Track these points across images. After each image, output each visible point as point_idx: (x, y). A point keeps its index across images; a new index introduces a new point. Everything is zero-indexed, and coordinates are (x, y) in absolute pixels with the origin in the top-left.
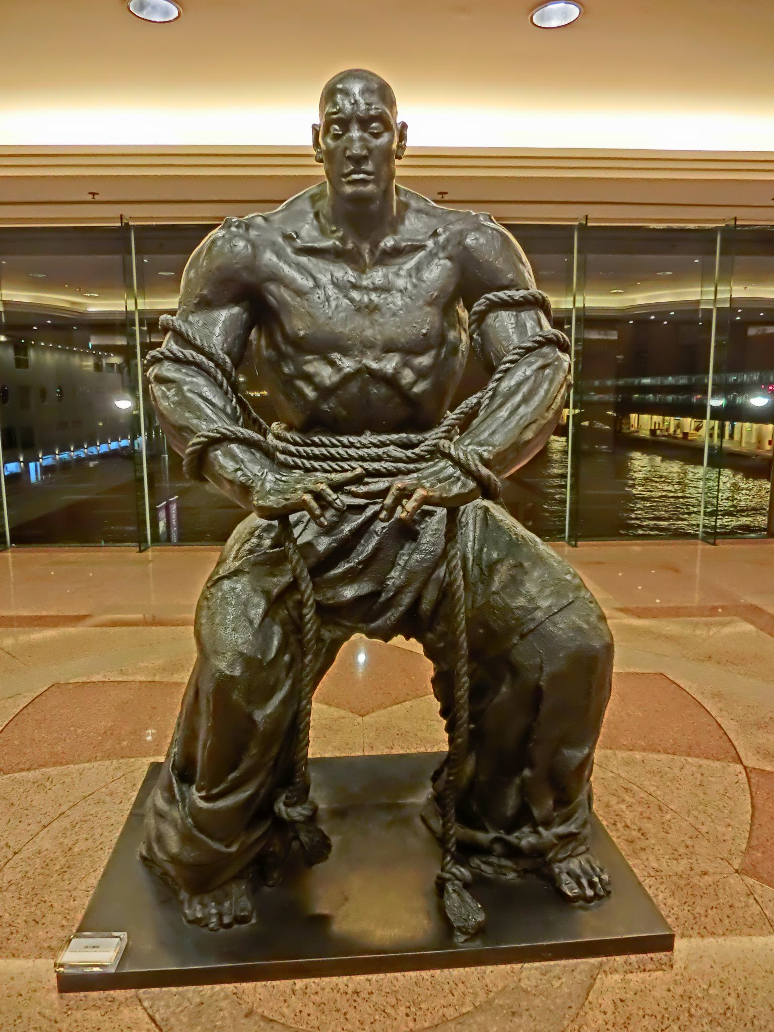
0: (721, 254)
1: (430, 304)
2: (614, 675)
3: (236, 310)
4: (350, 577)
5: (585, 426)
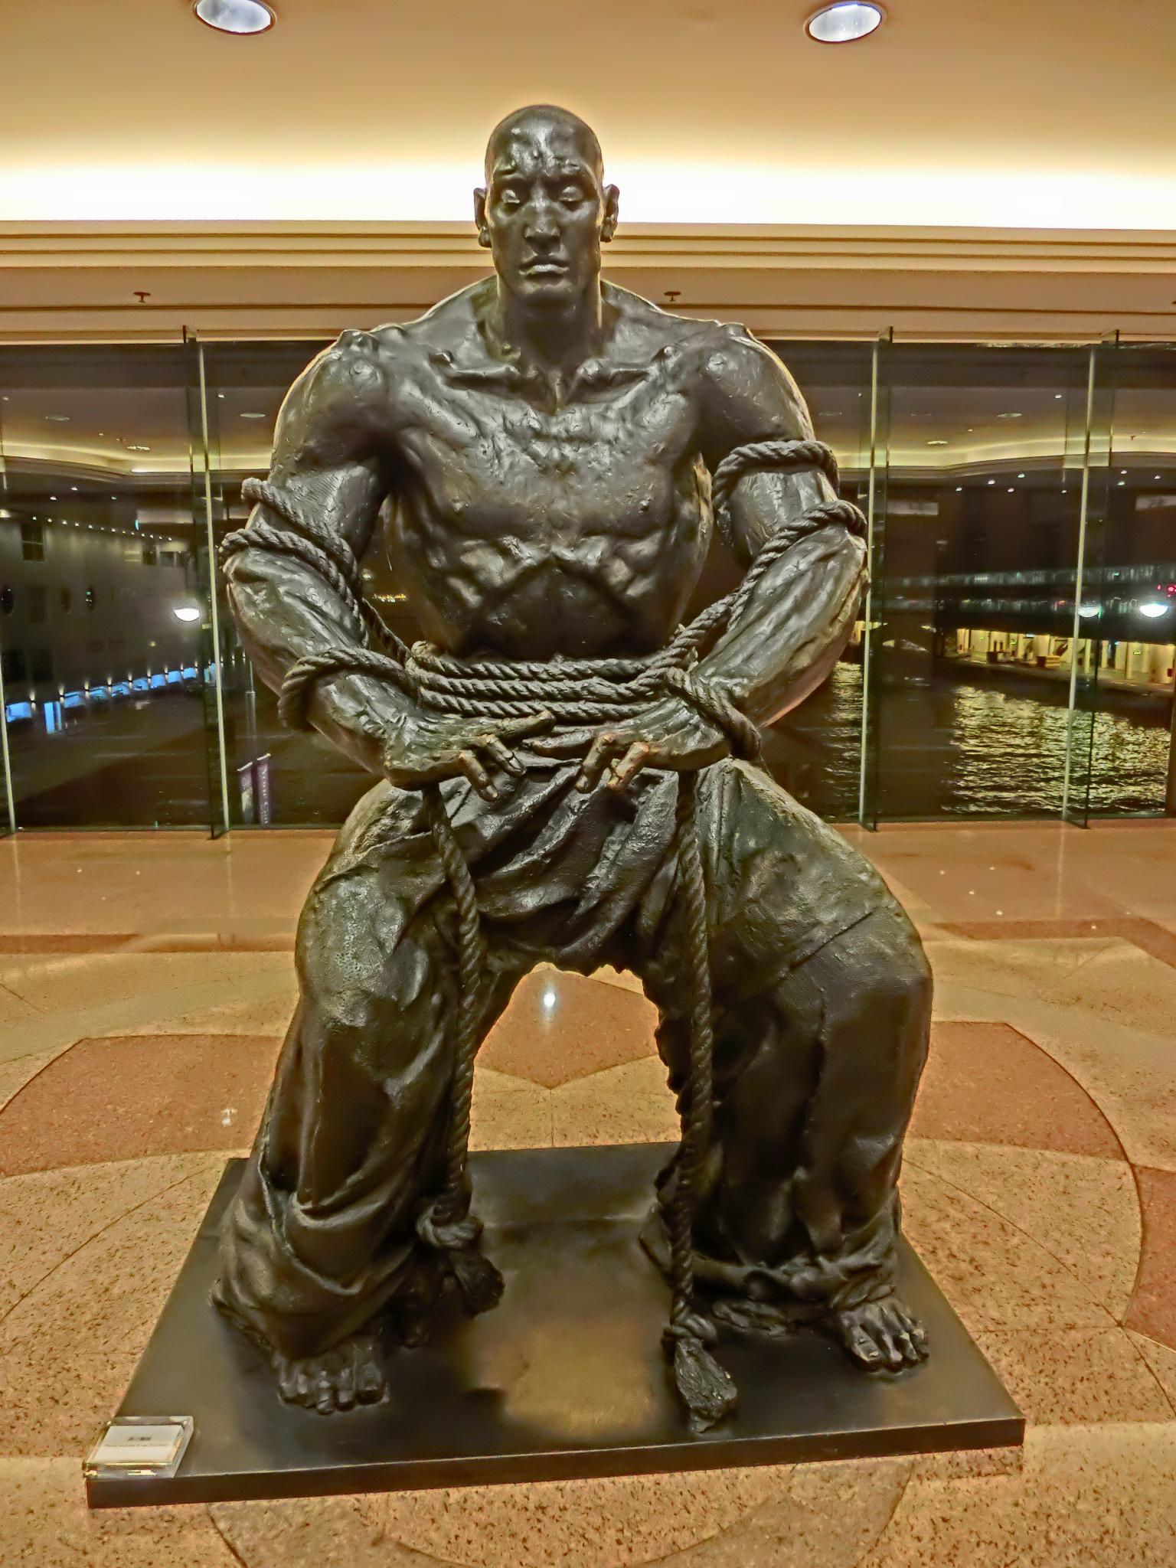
0: (1095, 386)
1: (653, 462)
3: (358, 471)
4: (532, 877)
5: (889, 647)
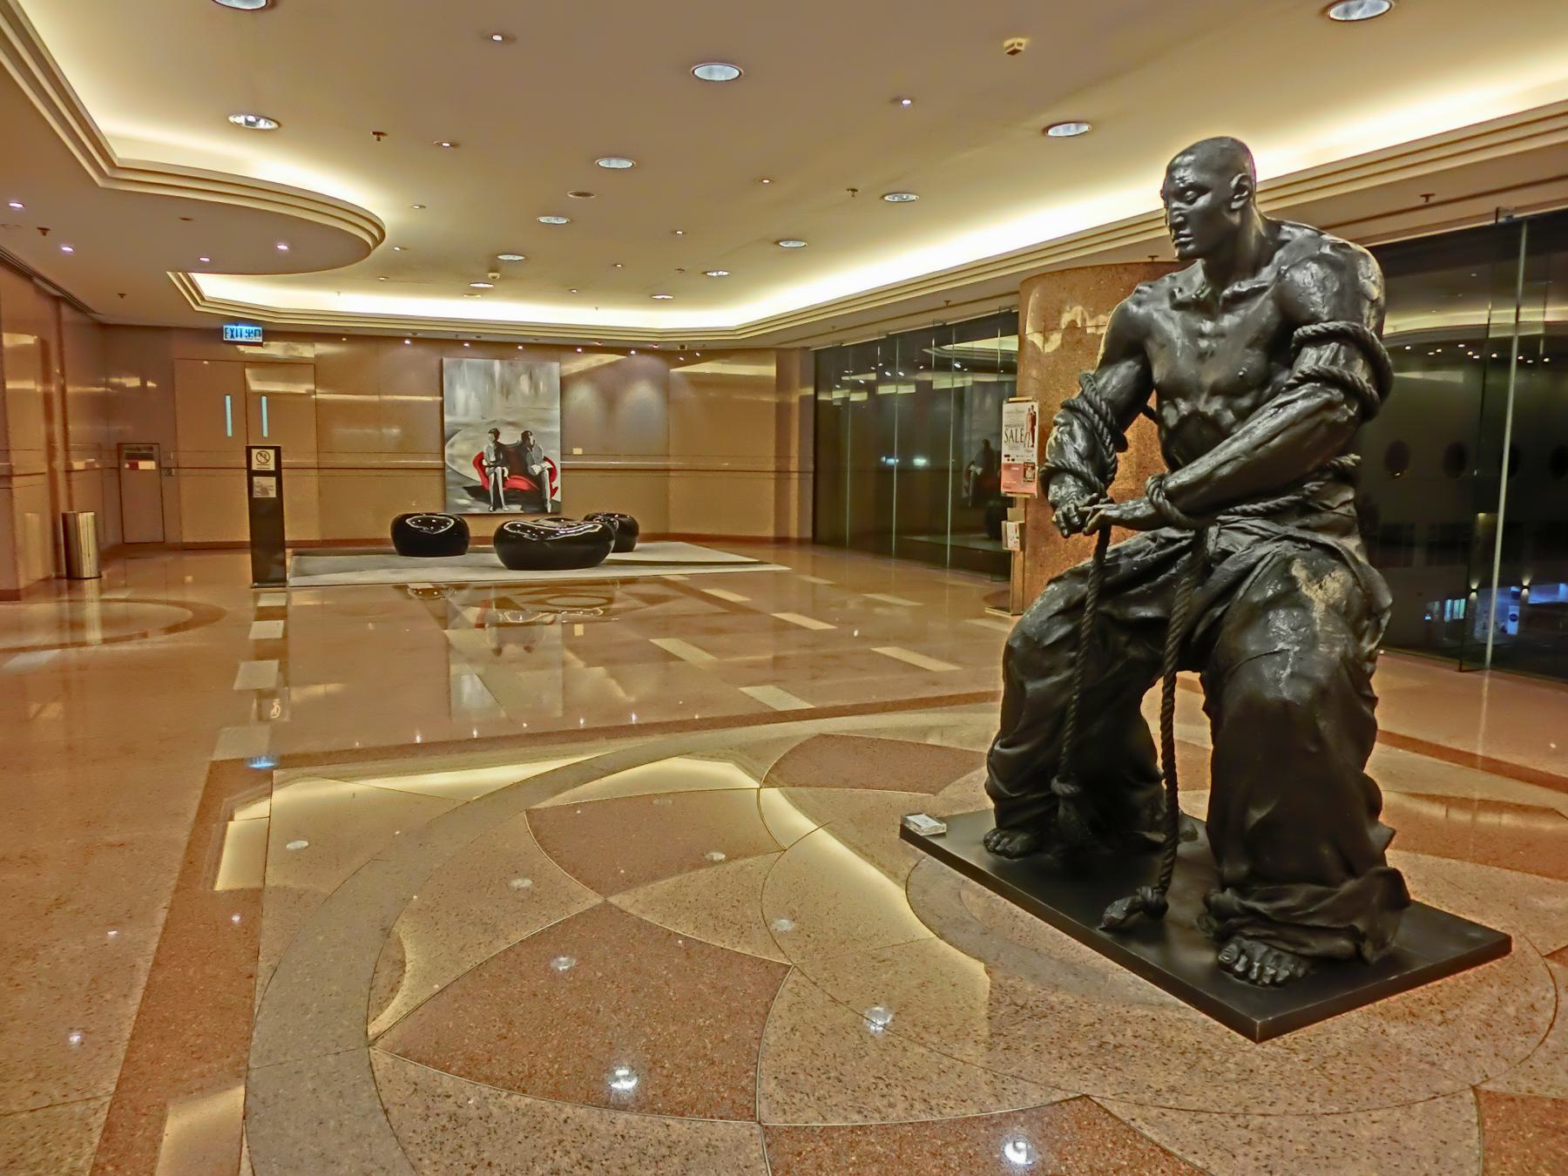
0: (1528, 254)
1: (1250, 345)
2: (1378, 734)
3: (1130, 363)
4: (1142, 600)
5: (153, 382)
